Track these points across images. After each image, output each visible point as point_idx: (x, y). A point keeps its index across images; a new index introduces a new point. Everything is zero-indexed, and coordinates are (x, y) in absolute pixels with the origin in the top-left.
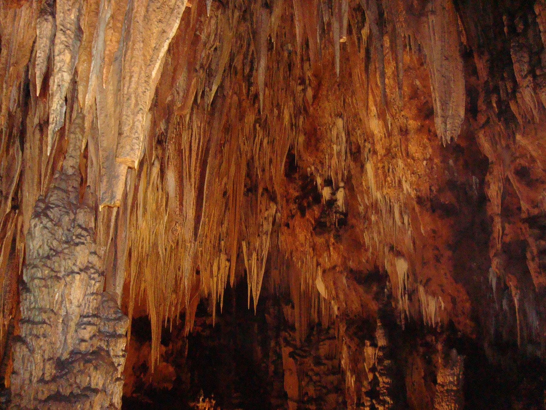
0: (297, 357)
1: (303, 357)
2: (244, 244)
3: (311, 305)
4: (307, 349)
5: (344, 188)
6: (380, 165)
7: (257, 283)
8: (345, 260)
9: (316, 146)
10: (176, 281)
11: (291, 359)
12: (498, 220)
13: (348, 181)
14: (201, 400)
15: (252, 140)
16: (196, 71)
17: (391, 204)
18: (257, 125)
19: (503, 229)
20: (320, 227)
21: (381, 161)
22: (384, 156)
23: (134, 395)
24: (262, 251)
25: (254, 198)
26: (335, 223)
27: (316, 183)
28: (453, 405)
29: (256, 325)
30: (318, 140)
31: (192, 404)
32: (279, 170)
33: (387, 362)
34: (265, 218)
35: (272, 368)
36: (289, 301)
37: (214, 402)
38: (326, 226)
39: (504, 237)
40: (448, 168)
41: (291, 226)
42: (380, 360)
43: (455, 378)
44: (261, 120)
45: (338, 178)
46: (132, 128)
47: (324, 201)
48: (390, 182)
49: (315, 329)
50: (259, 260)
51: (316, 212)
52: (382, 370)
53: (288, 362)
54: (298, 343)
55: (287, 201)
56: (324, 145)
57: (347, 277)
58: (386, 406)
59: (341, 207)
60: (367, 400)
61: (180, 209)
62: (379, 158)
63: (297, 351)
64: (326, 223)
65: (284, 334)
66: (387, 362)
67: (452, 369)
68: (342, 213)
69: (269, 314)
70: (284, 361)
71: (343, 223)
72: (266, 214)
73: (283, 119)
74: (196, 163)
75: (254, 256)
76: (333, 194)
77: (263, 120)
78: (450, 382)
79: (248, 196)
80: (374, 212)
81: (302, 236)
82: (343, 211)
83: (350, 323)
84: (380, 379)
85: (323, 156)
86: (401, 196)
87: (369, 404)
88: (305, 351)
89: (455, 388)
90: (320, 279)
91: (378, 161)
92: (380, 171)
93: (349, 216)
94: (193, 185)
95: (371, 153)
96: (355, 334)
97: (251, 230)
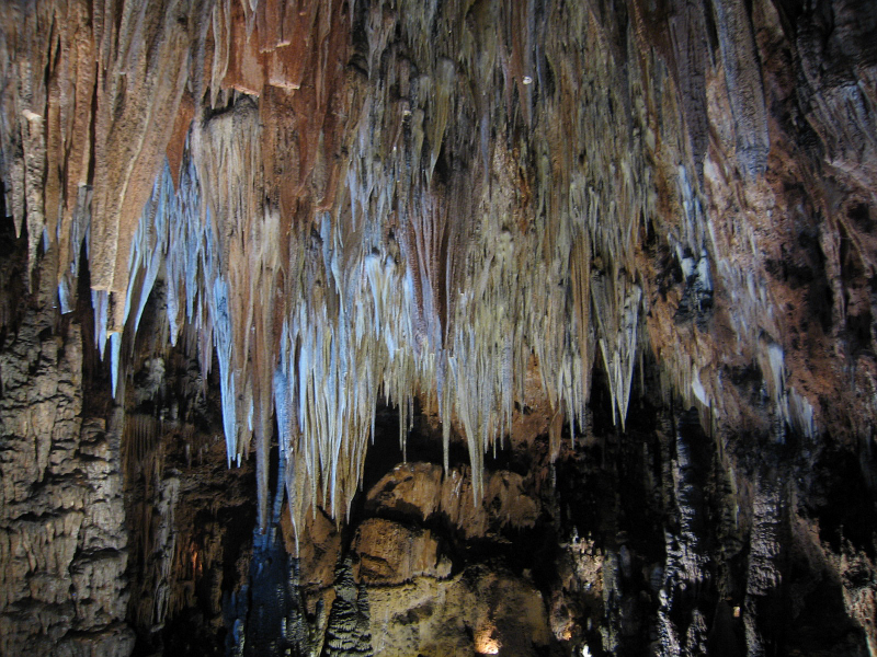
2: (602, 342)
6: (721, 223)
7: (624, 392)
8: (717, 353)
12: (837, 284)
14: (574, 540)
15: (585, 210)
16: (337, 156)
18: (590, 189)
19: (847, 297)
21: (723, 217)
23: (488, 535)
24: (626, 350)
25: (608, 282)
27: (676, 256)
28: (772, 544)
29: (645, 445)
30: (669, 198)
31: (563, 545)
32: (632, 239)
34: (626, 307)
37: (592, 542)
38: (687, 311)
39: (849, 308)
40: (797, 217)
41: (654, 315)
43: (775, 507)
46: (102, 255)
47: (685, 280)
50: (624, 361)
52: (682, 497)
57: (721, 377)
62: (720, 213)
66: (688, 487)
67: (770, 495)
68: (706, 292)
69: (661, 429)
71: (707, 305)
72: (628, 302)
73: (623, 176)
74: (431, 256)
75: (616, 356)
76: (695, 267)
78: (768, 513)
79: (601, 281)
81: (666, 325)
83: (732, 437)
85: (678, 218)
86: (753, 262)
89: (774, 521)
91: (719, 219)
92: (722, 232)
93: (715, 295)
96: (735, 452)
97: (609, 324)
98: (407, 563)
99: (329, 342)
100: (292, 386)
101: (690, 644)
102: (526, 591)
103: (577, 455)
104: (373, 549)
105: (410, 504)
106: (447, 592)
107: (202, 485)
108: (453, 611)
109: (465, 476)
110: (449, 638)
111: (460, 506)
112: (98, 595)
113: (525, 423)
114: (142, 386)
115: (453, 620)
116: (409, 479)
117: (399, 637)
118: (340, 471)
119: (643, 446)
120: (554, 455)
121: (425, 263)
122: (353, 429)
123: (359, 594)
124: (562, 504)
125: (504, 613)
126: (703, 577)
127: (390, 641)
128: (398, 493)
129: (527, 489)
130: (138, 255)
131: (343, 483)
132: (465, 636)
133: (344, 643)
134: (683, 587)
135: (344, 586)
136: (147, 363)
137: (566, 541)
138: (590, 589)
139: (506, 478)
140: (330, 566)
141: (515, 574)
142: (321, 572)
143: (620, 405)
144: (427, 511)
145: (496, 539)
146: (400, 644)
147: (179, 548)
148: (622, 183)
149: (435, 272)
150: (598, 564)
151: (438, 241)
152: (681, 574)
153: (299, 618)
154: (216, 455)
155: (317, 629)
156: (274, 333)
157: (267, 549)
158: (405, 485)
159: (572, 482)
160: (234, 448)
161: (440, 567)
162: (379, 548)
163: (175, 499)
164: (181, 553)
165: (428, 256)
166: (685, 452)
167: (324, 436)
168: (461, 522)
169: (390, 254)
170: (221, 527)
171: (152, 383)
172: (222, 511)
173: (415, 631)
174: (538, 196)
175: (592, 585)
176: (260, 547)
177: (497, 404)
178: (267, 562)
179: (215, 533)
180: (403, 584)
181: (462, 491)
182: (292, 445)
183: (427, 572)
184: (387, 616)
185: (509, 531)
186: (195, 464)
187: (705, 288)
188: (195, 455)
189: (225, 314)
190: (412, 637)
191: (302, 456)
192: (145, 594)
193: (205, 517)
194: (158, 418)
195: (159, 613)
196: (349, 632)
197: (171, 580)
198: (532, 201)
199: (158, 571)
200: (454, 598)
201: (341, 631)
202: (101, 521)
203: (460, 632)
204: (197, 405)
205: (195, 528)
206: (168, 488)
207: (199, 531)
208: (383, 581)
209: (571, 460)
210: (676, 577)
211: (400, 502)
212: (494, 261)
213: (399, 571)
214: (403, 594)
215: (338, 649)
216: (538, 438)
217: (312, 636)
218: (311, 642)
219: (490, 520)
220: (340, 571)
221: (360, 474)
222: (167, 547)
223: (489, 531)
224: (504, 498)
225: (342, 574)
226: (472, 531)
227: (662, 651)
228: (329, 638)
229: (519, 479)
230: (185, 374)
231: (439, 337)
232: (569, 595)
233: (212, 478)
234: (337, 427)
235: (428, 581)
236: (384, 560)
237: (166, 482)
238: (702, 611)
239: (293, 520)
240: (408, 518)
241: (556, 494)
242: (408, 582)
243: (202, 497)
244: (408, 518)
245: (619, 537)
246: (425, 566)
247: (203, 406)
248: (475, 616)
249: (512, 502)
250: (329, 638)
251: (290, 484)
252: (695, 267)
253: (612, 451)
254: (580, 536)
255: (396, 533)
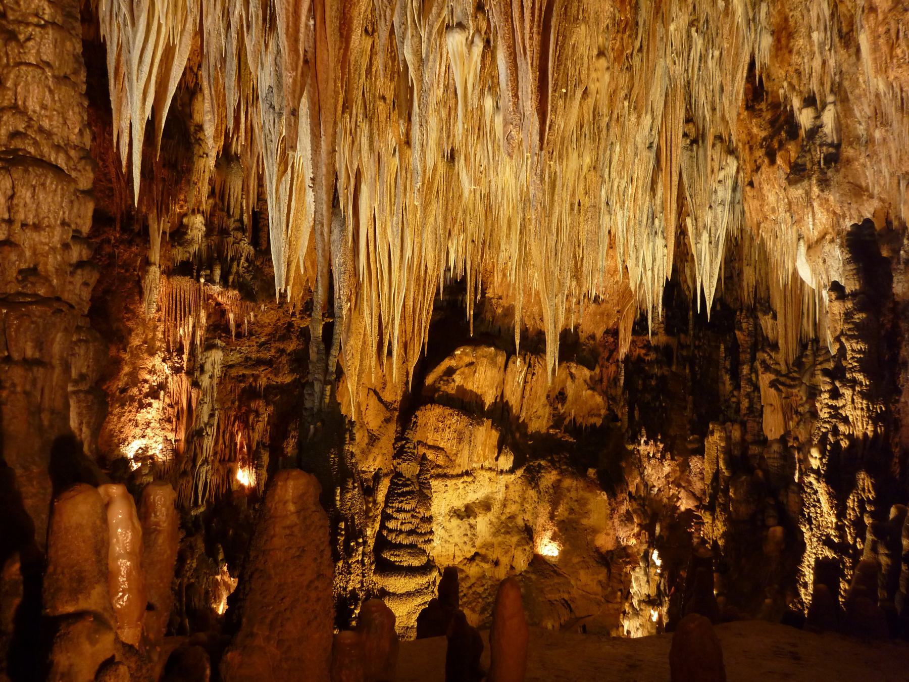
0: (780, 387)
1: (790, 386)
2: (689, 221)
3: (803, 313)
4: (795, 375)
5: (834, 103)
6: (881, 30)
7: (711, 276)
9: (787, 46)
10: (576, 263)
11: (773, 390)
13: (838, 90)
14: (642, 441)
15: (686, 54)
17: (904, 94)
18: (693, 29)
20: (797, 173)
21: (885, 21)
22: (890, 11)
23: (551, 431)
26: (819, 162)
29: (722, 347)
31: (630, 447)
33: (859, 317)
34: (720, 182)
35: (745, 403)
36: (768, 308)
37: (662, 446)
41: (756, 184)
42: (848, 316)
44: (699, 22)
45: (824, 91)
47: (802, 133)
48: (901, 55)
49: (809, 347)
51: (793, 154)
53: (769, 395)
54: (783, 368)
55: (751, 148)
56: (801, 42)
58: (858, 389)
59: (830, 135)
60: (825, 383)
61: (514, 103)
62: (880, 17)
63: (782, 379)
64: (804, 165)
65: (761, 355)
68: (831, 145)
69: (741, 329)
70: (762, 393)
72: (721, 176)
74: (531, 28)
75: (705, 237)
76: (818, 117)
77: (702, 22)
79: (692, 150)
80: (878, 123)
82: (833, 142)
84: (848, 346)
87: (828, 388)
88: (794, 379)
90: (804, 260)
91: (877, 25)
92: (882, 41)
94: (529, 62)
95: (866, 11)
98: (466, 453)
99: (393, 176)
100: (350, 228)
101: (851, 515)
102: (590, 491)
103: (646, 355)
104: (430, 438)
105: (471, 391)
106: (507, 487)
107: (247, 359)
108: (512, 508)
109: (529, 366)
110: (508, 536)
111: (523, 397)
112: (27, 239)
113: (595, 314)
114: (180, 245)
115: (512, 518)
116: (471, 364)
117: (456, 533)
118: (403, 332)
119: (719, 347)
120: (623, 350)
121: (523, 39)
122: (419, 285)
123: (421, 470)
124: (631, 405)
125: (566, 514)
126: (875, 431)
127: (446, 536)
128: (458, 379)
129: (593, 385)
130: (163, 29)
131: (405, 346)
132: (525, 535)
133: (402, 524)
134: (844, 444)
135: (404, 460)
136: (185, 220)
137: (633, 443)
138: (657, 494)
139: (573, 370)
140: (384, 454)
141: (579, 472)
142: (374, 460)
143: (706, 291)
144: (489, 400)
145: (559, 436)
146: (456, 540)
147: (222, 427)
148: (733, 22)
149: (536, 49)
150: (667, 469)
151: (540, 9)
152: (842, 428)
153: (354, 488)
154: (262, 326)
155: (375, 502)
156: (341, 35)
157: (320, 410)
158: (466, 370)
159: (640, 382)
160: (284, 278)
161: (502, 459)
162: (437, 436)
163: (217, 372)
164: (224, 432)
165: (527, 27)
166: (857, 274)
167: (386, 288)
168: (523, 414)
169: (478, 31)
170: (268, 404)
171: (191, 242)
172: (268, 388)
173: (472, 527)
174: (637, 24)
175: (659, 490)
176: (312, 408)
177: (577, 271)
178: (319, 424)
179: (261, 410)
180: (462, 475)
181: (525, 382)
182: (349, 300)
183: (486, 465)
184: (444, 509)
185: (574, 429)
186: (239, 335)
187: (829, 141)
188: (238, 325)
189: (272, 107)
190: (469, 533)
191: (361, 313)
192: (185, 473)
193: (251, 393)
194: (199, 281)
195: (200, 495)
196: (408, 512)
197: (213, 461)
198: (631, 29)
199: (198, 450)
200: (514, 494)
201: (399, 510)
202: (33, 105)
203: (520, 531)
204: (241, 270)
205: (239, 407)
206: (209, 361)
207: (244, 409)
208: (440, 471)
209: (640, 359)
210: (835, 432)
211: (461, 389)
212: (585, 92)
213: (458, 461)
214: (461, 486)
215: (396, 530)
216: (607, 332)
217: (369, 510)
218: (368, 517)
219: (554, 416)
220: (399, 444)
221: (425, 337)
222: (209, 424)
223: (552, 427)
224: (570, 391)
225: (403, 447)
226: (534, 426)
227: (810, 523)
228: (386, 517)
229: (586, 372)
230: (229, 234)
231: (536, 138)
232: (635, 500)
233: (258, 352)
234: (400, 277)
235: (488, 475)
236: (442, 449)
237: (208, 354)
238: (870, 474)
239: (349, 386)
240: (467, 405)
241: (623, 393)
242: (467, 473)
243: (247, 372)
244: (467, 405)
245: (691, 442)
246: (486, 458)
247: (248, 272)
248: (536, 516)
249: (578, 397)
250: (386, 517)
251: (345, 344)
252: (818, 117)
253: (684, 353)
254: (649, 438)
255: (456, 421)
